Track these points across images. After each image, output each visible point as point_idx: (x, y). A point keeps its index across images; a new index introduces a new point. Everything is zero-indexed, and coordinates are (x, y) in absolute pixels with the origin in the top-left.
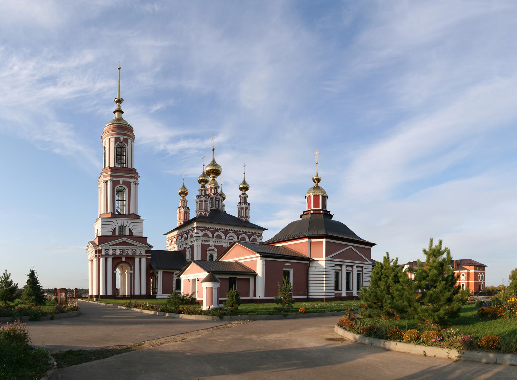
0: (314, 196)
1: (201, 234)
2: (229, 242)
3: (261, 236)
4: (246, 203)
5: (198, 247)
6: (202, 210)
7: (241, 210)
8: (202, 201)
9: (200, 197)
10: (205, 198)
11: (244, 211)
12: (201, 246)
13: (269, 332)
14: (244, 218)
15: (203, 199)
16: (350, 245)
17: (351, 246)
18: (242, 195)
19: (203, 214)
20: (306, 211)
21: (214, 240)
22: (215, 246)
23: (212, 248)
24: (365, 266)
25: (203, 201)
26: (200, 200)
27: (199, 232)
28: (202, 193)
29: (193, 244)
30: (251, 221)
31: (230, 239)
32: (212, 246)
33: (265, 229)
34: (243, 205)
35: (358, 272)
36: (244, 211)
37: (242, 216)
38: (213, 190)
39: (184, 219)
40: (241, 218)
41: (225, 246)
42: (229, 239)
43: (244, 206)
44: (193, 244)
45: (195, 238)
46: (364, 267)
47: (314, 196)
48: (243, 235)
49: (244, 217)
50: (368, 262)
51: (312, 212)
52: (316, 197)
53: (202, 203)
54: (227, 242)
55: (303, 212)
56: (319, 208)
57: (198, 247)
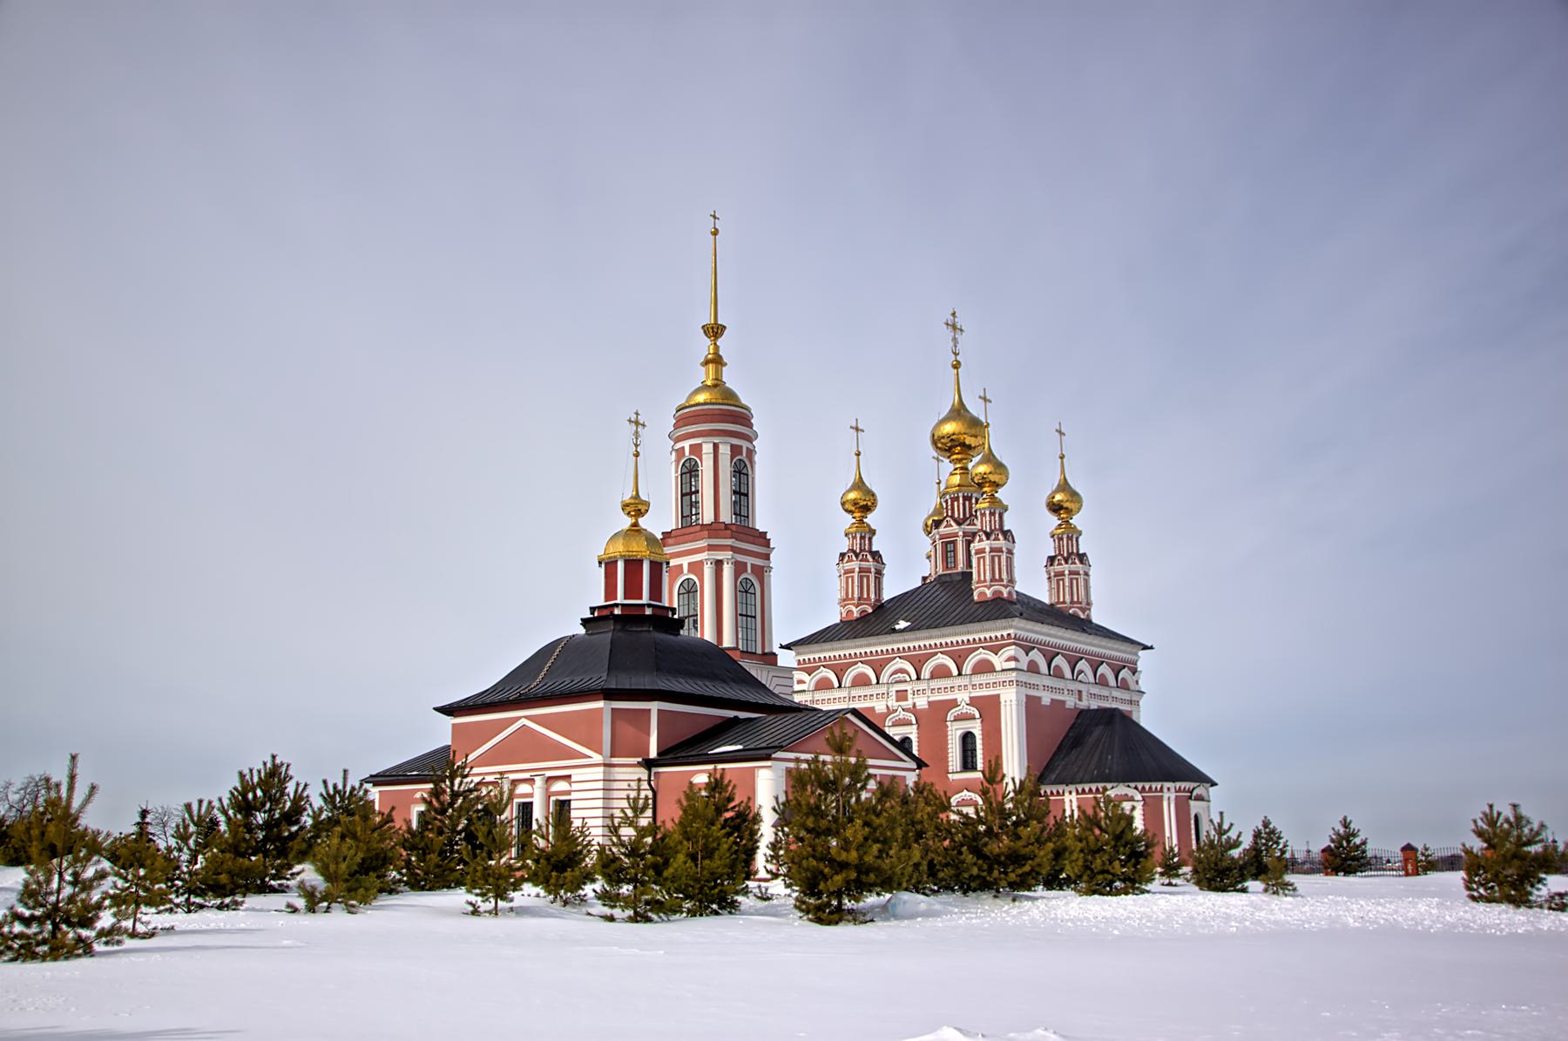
0: (651, 562)
2: (894, 693)
8: (852, 571)
10: (861, 561)
15: (855, 565)
16: (520, 718)
17: (523, 720)
20: (600, 608)
22: (974, 702)
23: (964, 708)
24: (576, 775)
25: (853, 572)
26: (846, 568)
30: (1097, 618)
32: (963, 703)
33: (1145, 648)
36: (987, 562)
37: (996, 581)
38: (958, 506)
39: (876, 600)
40: (1071, 608)
46: (573, 779)
47: (651, 562)
50: (590, 757)
51: (617, 611)
52: (633, 565)
53: (868, 578)
54: (885, 692)
55: (591, 608)
56: (641, 598)
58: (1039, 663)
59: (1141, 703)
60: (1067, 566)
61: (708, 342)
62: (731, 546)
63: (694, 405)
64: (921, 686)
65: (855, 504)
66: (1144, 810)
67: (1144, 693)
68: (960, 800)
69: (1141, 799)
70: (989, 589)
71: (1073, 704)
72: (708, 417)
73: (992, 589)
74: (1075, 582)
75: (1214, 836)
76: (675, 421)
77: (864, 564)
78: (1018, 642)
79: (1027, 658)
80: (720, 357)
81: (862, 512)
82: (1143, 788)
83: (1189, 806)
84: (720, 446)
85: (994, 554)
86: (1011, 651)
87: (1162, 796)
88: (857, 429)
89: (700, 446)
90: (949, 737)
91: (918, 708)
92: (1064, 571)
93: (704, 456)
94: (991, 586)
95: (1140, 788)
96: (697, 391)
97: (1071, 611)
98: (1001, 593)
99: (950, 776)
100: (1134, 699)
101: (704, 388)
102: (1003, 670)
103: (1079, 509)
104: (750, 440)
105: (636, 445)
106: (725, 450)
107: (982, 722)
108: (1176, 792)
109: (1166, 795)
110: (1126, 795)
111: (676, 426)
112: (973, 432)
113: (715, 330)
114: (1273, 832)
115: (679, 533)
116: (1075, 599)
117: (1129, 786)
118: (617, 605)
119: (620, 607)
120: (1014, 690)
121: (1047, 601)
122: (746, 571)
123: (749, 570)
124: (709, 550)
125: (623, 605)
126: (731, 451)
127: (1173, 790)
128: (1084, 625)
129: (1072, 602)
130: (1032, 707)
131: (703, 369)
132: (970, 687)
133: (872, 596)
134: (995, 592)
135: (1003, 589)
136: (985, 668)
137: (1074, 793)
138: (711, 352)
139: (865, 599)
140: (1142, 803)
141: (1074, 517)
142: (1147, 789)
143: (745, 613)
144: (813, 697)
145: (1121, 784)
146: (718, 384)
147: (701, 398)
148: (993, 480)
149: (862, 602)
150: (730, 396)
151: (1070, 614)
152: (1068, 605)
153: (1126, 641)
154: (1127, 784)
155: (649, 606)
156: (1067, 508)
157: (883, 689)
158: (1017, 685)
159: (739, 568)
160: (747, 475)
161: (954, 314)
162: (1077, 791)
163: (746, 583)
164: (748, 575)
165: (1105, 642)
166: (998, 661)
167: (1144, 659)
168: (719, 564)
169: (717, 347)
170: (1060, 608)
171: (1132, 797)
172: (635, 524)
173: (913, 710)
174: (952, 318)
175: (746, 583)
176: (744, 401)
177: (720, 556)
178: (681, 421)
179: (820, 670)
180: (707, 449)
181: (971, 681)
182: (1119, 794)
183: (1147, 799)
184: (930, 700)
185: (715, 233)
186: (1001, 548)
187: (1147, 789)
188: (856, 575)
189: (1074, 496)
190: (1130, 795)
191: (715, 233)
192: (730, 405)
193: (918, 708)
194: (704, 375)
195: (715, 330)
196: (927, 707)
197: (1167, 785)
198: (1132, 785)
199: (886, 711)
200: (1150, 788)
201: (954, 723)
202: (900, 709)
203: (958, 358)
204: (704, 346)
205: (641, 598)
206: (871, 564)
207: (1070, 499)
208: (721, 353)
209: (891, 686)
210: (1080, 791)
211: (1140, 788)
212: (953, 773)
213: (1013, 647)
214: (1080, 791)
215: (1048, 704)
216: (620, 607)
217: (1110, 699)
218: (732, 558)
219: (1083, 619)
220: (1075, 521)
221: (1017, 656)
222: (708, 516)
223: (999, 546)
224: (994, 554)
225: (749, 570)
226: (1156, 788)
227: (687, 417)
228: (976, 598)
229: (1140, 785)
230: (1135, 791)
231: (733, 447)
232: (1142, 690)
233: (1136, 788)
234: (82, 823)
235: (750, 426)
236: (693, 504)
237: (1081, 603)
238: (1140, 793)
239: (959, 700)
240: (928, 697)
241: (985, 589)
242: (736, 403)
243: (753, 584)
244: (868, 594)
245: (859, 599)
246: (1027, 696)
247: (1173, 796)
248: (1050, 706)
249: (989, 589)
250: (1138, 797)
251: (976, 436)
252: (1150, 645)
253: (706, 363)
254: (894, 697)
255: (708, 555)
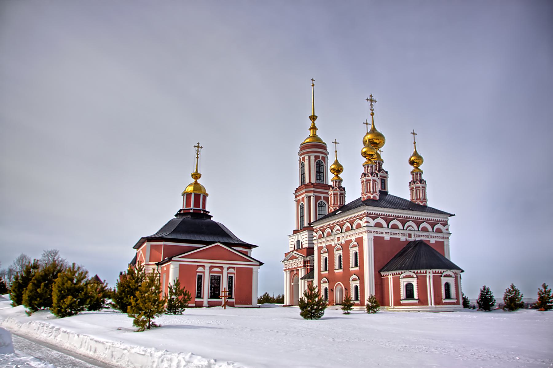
1: (373, 223)
3: (447, 224)
4: (421, 181)
5: (370, 241)
6: (370, 192)
7: (417, 190)
9: (367, 175)
11: (371, 185)
12: (374, 239)
13: (510, 361)
14: (365, 195)
18: (415, 171)
19: (372, 197)
21: (388, 230)
27: (370, 220)
28: (367, 170)
29: (362, 237)
30: (429, 205)
31: (409, 230)
33: (451, 215)
34: (368, 176)
35: (229, 275)
36: (371, 185)
37: (369, 192)
39: (340, 204)
40: (416, 201)
41: (433, 241)
42: (408, 229)
43: (419, 185)
44: (362, 237)
45: (366, 229)
48: (424, 223)
49: (422, 200)
51: (191, 211)
56: (199, 207)
57: (370, 241)
58: (426, 226)
59: (450, 238)
60: (414, 185)
61: (311, 122)
62: (314, 191)
63: (306, 143)
64: (343, 235)
65: (334, 170)
66: (417, 281)
67: (451, 234)
68: (353, 278)
69: (454, 276)
70: (365, 196)
71: (405, 239)
72: (307, 147)
73: (373, 195)
74: (418, 191)
75: (323, 296)
76: (300, 149)
77: (335, 192)
78: (369, 215)
79: (374, 221)
80: (316, 127)
81: (337, 173)
82: (417, 272)
83: (441, 279)
84: (311, 157)
85: (367, 182)
86: (365, 219)
87: (426, 275)
88: (336, 143)
89: (304, 157)
90: (350, 254)
91: (343, 243)
92: (413, 187)
93: (306, 161)
94: (366, 194)
95: (416, 272)
96: (307, 138)
97: (416, 203)
98: (370, 197)
99: (350, 269)
100: (445, 236)
101: (310, 137)
102: (363, 227)
103: (422, 162)
104: (326, 155)
105: (198, 155)
106: (313, 158)
107: (359, 248)
108: (433, 273)
109: (428, 275)
110: (410, 275)
111: (300, 151)
112: (377, 138)
113: (314, 118)
114: (516, 291)
115: (300, 188)
116: (418, 198)
117: (411, 272)
118: (191, 209)
119: (192, 210)
120: (367, 234)
121: (409, 198)
122: (321, 199)
123: (322, 198)
124: (306, 193)
125: (193, 209)
126: (315, 158)
127: (431, 273)
128: (424, 208)
129: (417, 199)
130: (378, 242)
131: (310, 131)
132: (355, 234)
133: (339, 203)
134: (368, 197)
135: (371, 195)
136: (359, 226)
137: (391, 275)
138: (312, 125)
139: (336, 204)
140: (454, 278)
141: (420, 166)
142: (419, 273)
143: (321, 214)
144: (318, 241)
145: (407, 271)
146: (315, 136)
147: (308, 140)
148: (369, 154)
149: (335, 205)
150: (319, 140)
151: (416, 204)
152: (415, 200)
153: (445, 214)
154: (410, 271)
155: (202, 210)
156: (416, 163)
157: (333, 237)
158: (368, 232)
159: (317, 198)
160: (323, 166)
161: (371, 96)
162: (433, 272)
163: (322, 203)
164: (322, 200)
165: (433, 215)
166: (363, 223)
167: (450, 220)
168: (309, 197)
169: (314, 123)
170: (413, 202)
171: (413, 276)
172: (196, 182)
173: (341, 245)
174: (370, 97)
175: (322, 203)
176: (324, 141)
177: (309, 194)
178: (302, 148)
179: (318, 232)
180: (307, 158)
181: (355, 232)
182: (407, 275)
183: (419, 277)
184: (345, 240)
185: (313, 85)
186: (370, 179)
187: (419, 273)
188: (332, 196)
189: (420, 158)
190: (412, 275)
191: (313, 85)
192: (319, 142)
193: (343, 243)
194: (310, 133)
195: (314, 118)
196: (344, 243)
197: (428, 271)
198: (413, 271)
199: (334, 245)
200: (420, 272)
201: (351, 249)
202: (338, 245)
203: (373, 111)
204: (310, 123)
205: (199, 207)
206: (338, 191)
207: (418, 159)
208: (316, 125)
209: (335, 235)
210: (434, 272)
211: (416, 272)
212: (351, 268)
213: (366, 217)
214: (434, 272)
215: (389, 239)
216: (192, 210)
217: (430, 237)
218: (314, 195)
219: (422, 206)
220: (420, 167)
221: (368, 221)
222: (307, 181)
223: (369, 179)
224: (367, 182)
225: (322, 198)
226: (423, 272)
227: (304, 147)
228: (362, 200)
229: (416, 271)
230: (414, 274)
231: (315, 156)
232: (450, 232)
233: (414, 272)
234: (314, 286)
235: (326, 150)
236: (304, 178)
237: (421, 199)
238: (416, 274)
239: (352, 240)
240: (345, 239)
241: (364, 196)
242: (320, 142)
243: (325, 203)
244: (337, 202)
245: (334, 204)
246: (374, 236)
247: (431, 275)
248: (390, 240)
249: (365, 196)
250: (415, 276)
251: (378, 139)
252: (453, 214)
253: (310, 129)
254: (337, 240)
255: (305, 194)
